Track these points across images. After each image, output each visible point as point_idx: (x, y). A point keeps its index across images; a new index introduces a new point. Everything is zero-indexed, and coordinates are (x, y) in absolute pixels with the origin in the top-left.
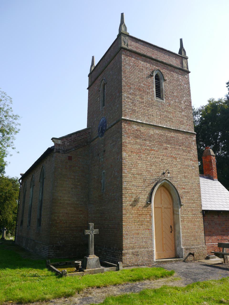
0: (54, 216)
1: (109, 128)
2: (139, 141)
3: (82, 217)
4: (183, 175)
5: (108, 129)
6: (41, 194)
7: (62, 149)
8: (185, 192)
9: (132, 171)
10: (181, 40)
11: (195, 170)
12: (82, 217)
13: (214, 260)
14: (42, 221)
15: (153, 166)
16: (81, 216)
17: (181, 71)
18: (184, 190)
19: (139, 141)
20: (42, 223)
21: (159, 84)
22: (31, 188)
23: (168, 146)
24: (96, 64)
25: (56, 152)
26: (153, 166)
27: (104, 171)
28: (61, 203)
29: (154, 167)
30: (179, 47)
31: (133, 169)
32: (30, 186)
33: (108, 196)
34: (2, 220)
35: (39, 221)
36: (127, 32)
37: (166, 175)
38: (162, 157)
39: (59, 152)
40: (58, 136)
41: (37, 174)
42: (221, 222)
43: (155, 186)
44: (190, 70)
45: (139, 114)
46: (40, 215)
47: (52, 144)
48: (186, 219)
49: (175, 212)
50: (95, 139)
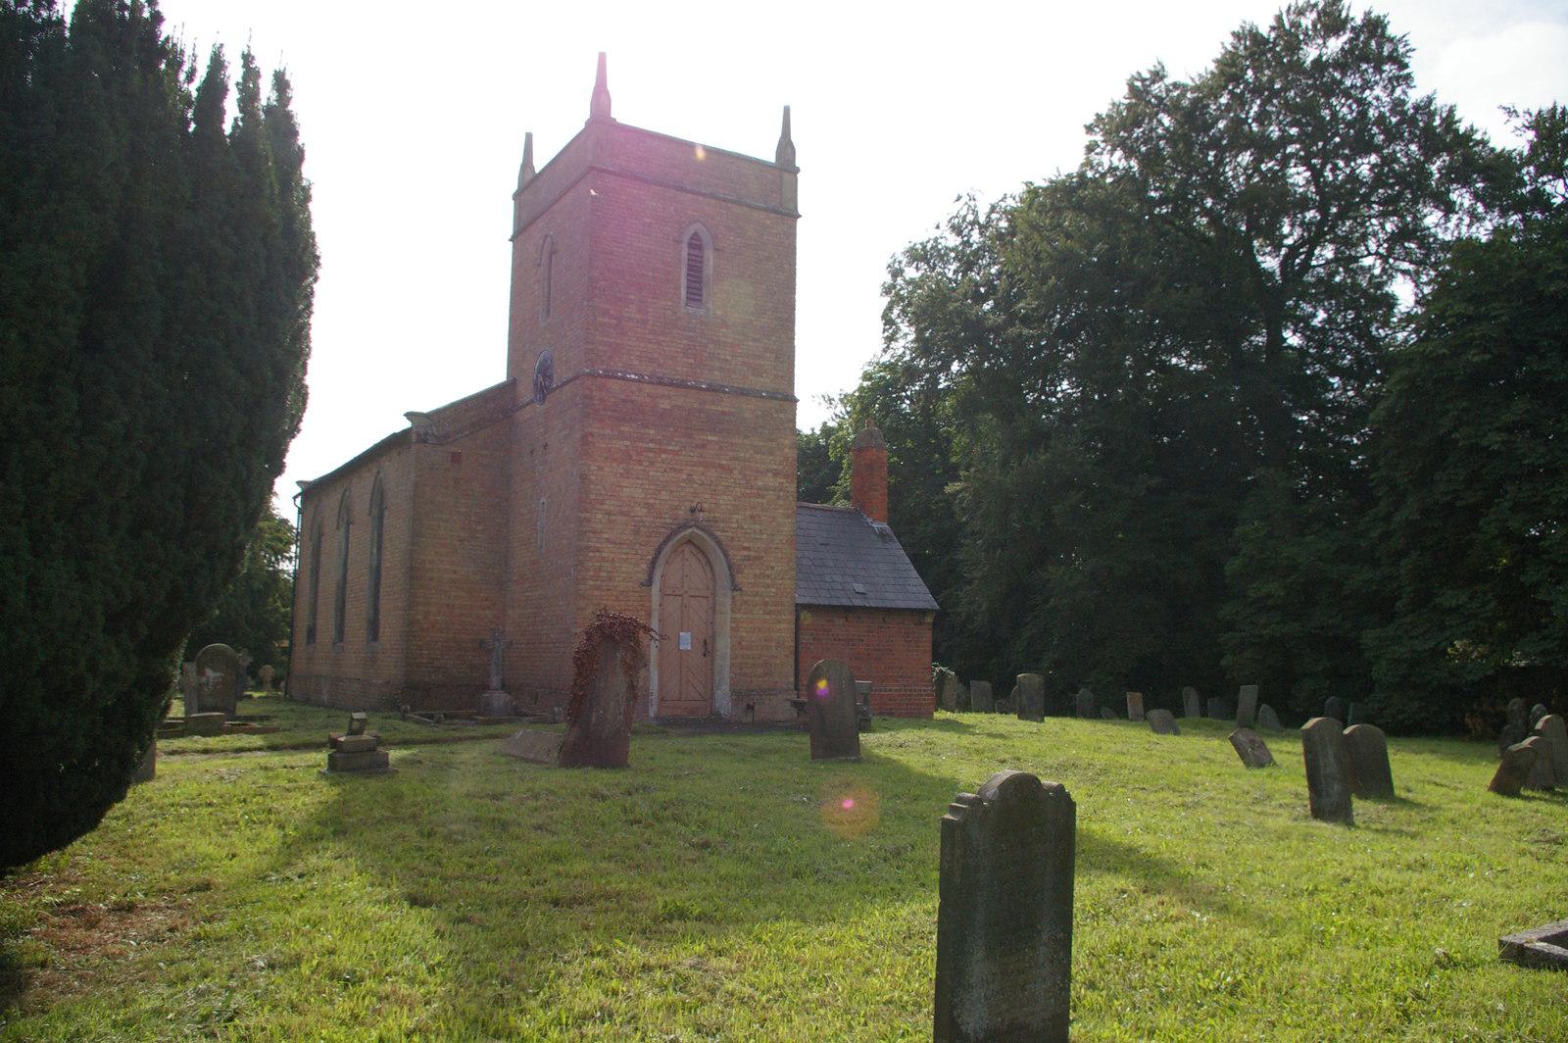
0: (414, 612)
1: (558, 387)
2: (627, 429)
3: (490, 616)
4: (748, 513)
5: (555, 389)
6: (375, 551)
7: (433, 434)
8: (748, 558)
9: (605, 507)
10: (787, 111)
11: (784, 500)
12: (490, 616)
13: (656, 672)
14: (381, 626)
15: (663, 493)
16: (487, 612)
17: (773, 215)
18: (745, 553)
19: (627, 429)
20: (381, 630)
21: (701, 262)
22: (343, 530)
23: (709, 438)
24: (539, 163)
25: (418, 442)
26: (663, 493)
27: (543, 500)
28: (431, 579)
29: (664, 495)
30: (778, 134)
31: (608, 502)
32: (338, 524)
33: (549, 564)
34: (1447, 352)
35: (374, 628)
36: (613, 115)
37: (697, 512)
38: (689, 468)
39: (425, 442)
40: (427, 406)
41: (361, 490)
42: (854, 635)
43: (665, 542)
44: (800, 212)
45: (632, 357)
46: (376, 610)
47: (407, 424)
48: (745, 625)
49: (717, 607)
50: (524, 406)
